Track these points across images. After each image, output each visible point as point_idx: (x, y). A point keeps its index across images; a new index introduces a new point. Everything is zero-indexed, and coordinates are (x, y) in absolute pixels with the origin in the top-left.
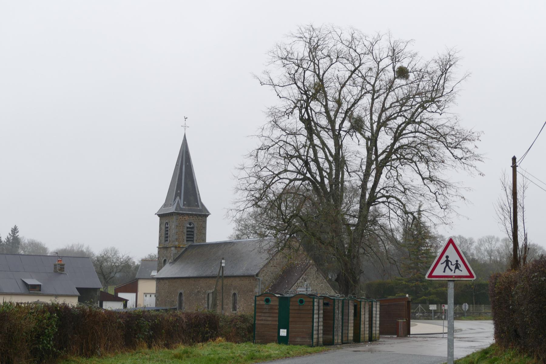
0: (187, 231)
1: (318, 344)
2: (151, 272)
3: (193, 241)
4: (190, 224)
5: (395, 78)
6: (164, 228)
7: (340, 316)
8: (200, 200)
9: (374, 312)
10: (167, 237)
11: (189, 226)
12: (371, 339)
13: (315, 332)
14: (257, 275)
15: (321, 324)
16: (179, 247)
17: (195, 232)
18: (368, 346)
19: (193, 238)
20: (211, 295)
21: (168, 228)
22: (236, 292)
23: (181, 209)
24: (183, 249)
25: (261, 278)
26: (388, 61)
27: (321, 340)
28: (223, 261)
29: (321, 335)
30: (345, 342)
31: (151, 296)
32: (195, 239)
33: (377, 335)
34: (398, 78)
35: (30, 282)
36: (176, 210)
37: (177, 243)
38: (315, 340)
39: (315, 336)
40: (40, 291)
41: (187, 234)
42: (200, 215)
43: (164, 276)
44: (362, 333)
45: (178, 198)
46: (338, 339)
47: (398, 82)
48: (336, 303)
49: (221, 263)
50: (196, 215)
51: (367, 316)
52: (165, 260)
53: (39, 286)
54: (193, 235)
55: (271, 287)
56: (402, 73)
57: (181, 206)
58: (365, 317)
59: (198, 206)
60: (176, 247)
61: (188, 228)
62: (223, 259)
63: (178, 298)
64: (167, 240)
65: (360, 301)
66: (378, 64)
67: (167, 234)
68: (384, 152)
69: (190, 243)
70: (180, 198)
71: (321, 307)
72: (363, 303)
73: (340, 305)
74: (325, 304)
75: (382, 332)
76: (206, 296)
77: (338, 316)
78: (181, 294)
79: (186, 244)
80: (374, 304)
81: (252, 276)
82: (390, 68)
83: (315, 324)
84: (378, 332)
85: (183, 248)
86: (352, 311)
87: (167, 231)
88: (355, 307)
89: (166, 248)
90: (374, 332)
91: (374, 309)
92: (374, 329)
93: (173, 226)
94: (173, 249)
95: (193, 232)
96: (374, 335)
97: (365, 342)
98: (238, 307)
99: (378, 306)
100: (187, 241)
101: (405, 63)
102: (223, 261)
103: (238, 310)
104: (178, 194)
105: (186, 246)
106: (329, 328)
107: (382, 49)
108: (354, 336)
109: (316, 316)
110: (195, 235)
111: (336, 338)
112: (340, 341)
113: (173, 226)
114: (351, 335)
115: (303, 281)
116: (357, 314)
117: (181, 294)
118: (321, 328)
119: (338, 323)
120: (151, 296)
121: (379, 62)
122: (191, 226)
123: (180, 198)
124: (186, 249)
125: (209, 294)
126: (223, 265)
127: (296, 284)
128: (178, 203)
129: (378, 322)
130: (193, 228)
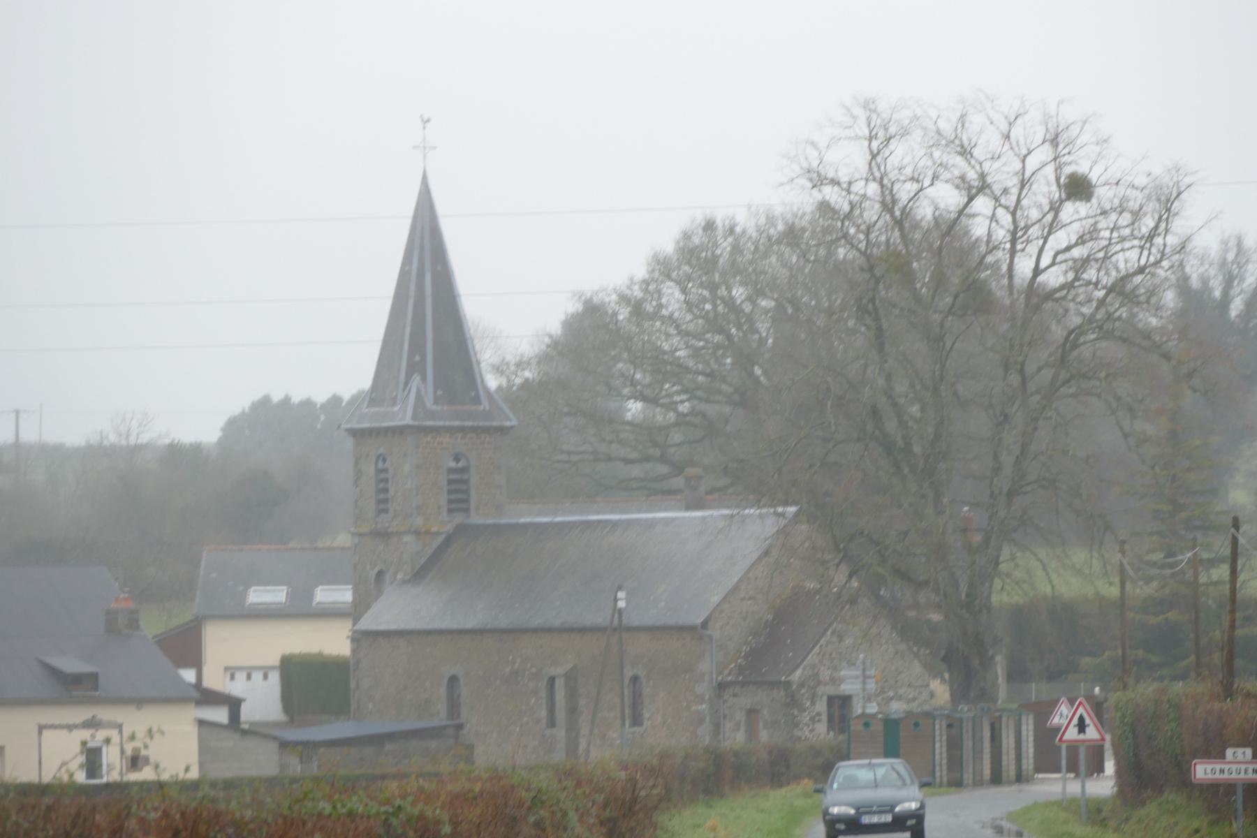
0: (450, 482)
1: (941, 785)
2: (244, 594)
3: (467, 510)
4: (457, 459)
5: (1062, 202)
6: (370, 469)
7: (970, 744)
8: (482, 381)
9: (1024, 733)
10: (386, 501)
11: (452, 464)
12: (1020, 778)
13: (937, 768)
14: (705, 625)
15: (945, 755)
16: (428, 532)
17: (474, 480)
18: (1015, 788)
19: (466, 501)
20: (560, 684)
21: (385, 471)
22: (641, 672)
23: (431, 415)
24: (440, 539)
25: (714, 632)
26: (1042, 154)
27: (945, 779)
28: (621, 595)
29: (945, 773)
30: (978, 783)
31: (249, 677)
32: (473, 503)
33: (1031, 773)
34: (1068, 198)
35: (72, 665)
36: (415, 417)
37: (419, 521)
38: (938, 780)
39: (938, 774)
40: (96, 689)
41: (450, 492)
42: (487, 430)
43: (393, 627)
44: (1004, 768)
45: (416, 380)
46: (968, 777)
47: (1071, 210)
48: (964, 724)
49: (616, 600)
50: (475, 430)
51: (1012, 740)
52: (380, 574)
53: (94, 677)
54: (467, 492)
55: (746, 657)
56: (1078, 188)
57: (429, 402)
58: (1008, 742)
59: (477, 400)
60: (418, 533)
61: (450, 470)
62: (620, 588)
63: (443, 691)
64: (386, 511)
65: (1000, 717)
66: (1023, 161)
67: (386, 490)
68: (1038, 392)
69: (459, 519)
70: (424, 379)
71: (944, 732)
72: (1004, 720)
73: (970, 725)
74: (949, 726)
75: (1038, 769)
76: (543, 684)
77: (968, 743)
78: (453, 680)
79: (445, 524)
80: (1024, 719)
81: (692, 629)
82: (1050, 171)
83: (937, 757)
84: (1031, 767)
85: (438, 533)
86: (987, 734)
87: (386, 481)
88: (993, 726)
89: (382, 535)
90: (1024, 767)
91: (1024, 727)
92: (1024, 761)
93: (407, 468)
94: (408, 538)
95: (466, 482)
96: (1024, 773)
97: (1009, 783)
98: (646, 714)
99: (1031, 721)
100: (450, 511)
101: (1081, 165)
102: (621, 595)
103: (647, 723)
104: (416, 367)
105: (449, 528)
106: (955, 762)
107: (1031, 132)
108: (992, 773)
109: (937, 745)
110: (473, 492)
111: (965, 776)
112: (971, 781)
113: (407, 468)
114: (987, 771)
115: (835, 639)
116: (995, 738)
117: (453, 680)
118: (945, 761)
119: (968, 754)
120: (249, 677)
121: (1025, 157)
122: (460, 464)
123: (424, 379)
124: (449, 540)
125: (552, 681)
126: (621, 604)
127: (817, 649)
128: (419, 397)
129: (1031, 750)
130: (464, 470)
